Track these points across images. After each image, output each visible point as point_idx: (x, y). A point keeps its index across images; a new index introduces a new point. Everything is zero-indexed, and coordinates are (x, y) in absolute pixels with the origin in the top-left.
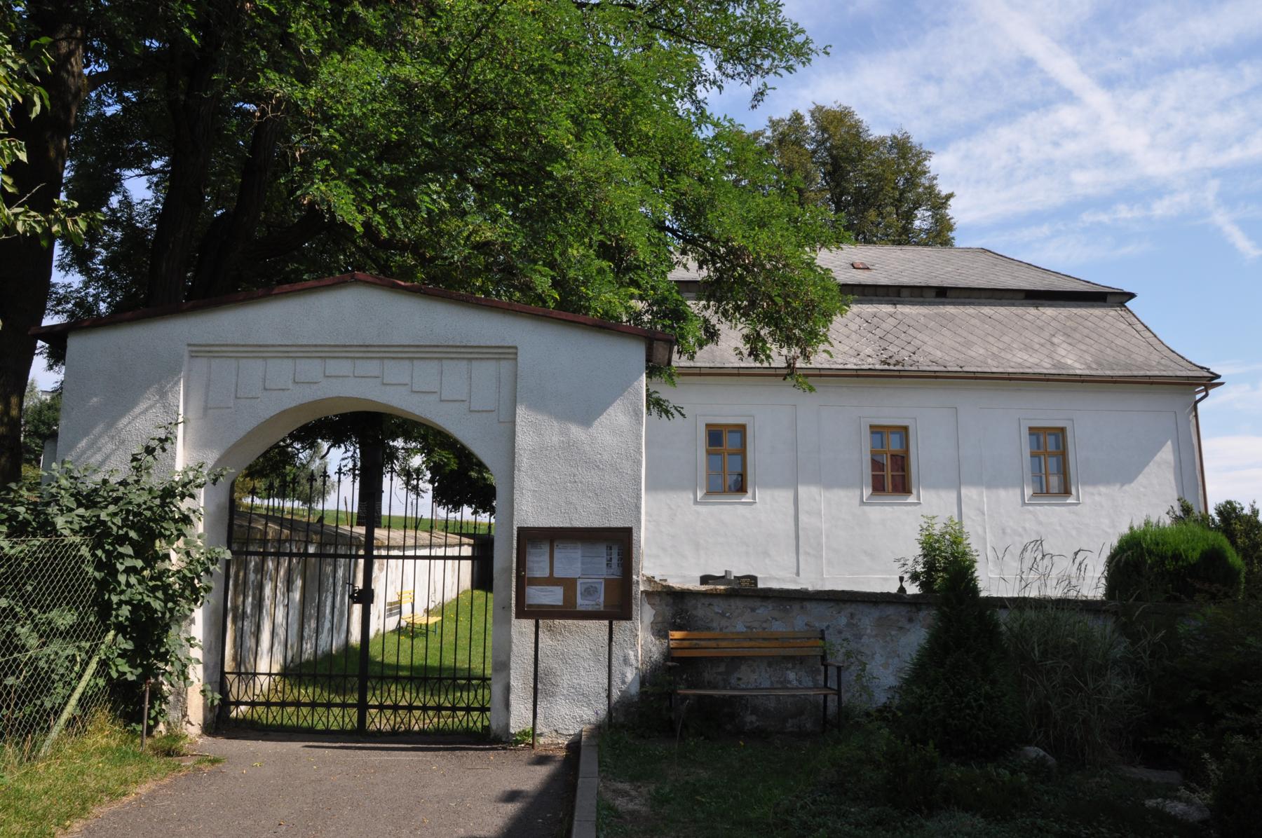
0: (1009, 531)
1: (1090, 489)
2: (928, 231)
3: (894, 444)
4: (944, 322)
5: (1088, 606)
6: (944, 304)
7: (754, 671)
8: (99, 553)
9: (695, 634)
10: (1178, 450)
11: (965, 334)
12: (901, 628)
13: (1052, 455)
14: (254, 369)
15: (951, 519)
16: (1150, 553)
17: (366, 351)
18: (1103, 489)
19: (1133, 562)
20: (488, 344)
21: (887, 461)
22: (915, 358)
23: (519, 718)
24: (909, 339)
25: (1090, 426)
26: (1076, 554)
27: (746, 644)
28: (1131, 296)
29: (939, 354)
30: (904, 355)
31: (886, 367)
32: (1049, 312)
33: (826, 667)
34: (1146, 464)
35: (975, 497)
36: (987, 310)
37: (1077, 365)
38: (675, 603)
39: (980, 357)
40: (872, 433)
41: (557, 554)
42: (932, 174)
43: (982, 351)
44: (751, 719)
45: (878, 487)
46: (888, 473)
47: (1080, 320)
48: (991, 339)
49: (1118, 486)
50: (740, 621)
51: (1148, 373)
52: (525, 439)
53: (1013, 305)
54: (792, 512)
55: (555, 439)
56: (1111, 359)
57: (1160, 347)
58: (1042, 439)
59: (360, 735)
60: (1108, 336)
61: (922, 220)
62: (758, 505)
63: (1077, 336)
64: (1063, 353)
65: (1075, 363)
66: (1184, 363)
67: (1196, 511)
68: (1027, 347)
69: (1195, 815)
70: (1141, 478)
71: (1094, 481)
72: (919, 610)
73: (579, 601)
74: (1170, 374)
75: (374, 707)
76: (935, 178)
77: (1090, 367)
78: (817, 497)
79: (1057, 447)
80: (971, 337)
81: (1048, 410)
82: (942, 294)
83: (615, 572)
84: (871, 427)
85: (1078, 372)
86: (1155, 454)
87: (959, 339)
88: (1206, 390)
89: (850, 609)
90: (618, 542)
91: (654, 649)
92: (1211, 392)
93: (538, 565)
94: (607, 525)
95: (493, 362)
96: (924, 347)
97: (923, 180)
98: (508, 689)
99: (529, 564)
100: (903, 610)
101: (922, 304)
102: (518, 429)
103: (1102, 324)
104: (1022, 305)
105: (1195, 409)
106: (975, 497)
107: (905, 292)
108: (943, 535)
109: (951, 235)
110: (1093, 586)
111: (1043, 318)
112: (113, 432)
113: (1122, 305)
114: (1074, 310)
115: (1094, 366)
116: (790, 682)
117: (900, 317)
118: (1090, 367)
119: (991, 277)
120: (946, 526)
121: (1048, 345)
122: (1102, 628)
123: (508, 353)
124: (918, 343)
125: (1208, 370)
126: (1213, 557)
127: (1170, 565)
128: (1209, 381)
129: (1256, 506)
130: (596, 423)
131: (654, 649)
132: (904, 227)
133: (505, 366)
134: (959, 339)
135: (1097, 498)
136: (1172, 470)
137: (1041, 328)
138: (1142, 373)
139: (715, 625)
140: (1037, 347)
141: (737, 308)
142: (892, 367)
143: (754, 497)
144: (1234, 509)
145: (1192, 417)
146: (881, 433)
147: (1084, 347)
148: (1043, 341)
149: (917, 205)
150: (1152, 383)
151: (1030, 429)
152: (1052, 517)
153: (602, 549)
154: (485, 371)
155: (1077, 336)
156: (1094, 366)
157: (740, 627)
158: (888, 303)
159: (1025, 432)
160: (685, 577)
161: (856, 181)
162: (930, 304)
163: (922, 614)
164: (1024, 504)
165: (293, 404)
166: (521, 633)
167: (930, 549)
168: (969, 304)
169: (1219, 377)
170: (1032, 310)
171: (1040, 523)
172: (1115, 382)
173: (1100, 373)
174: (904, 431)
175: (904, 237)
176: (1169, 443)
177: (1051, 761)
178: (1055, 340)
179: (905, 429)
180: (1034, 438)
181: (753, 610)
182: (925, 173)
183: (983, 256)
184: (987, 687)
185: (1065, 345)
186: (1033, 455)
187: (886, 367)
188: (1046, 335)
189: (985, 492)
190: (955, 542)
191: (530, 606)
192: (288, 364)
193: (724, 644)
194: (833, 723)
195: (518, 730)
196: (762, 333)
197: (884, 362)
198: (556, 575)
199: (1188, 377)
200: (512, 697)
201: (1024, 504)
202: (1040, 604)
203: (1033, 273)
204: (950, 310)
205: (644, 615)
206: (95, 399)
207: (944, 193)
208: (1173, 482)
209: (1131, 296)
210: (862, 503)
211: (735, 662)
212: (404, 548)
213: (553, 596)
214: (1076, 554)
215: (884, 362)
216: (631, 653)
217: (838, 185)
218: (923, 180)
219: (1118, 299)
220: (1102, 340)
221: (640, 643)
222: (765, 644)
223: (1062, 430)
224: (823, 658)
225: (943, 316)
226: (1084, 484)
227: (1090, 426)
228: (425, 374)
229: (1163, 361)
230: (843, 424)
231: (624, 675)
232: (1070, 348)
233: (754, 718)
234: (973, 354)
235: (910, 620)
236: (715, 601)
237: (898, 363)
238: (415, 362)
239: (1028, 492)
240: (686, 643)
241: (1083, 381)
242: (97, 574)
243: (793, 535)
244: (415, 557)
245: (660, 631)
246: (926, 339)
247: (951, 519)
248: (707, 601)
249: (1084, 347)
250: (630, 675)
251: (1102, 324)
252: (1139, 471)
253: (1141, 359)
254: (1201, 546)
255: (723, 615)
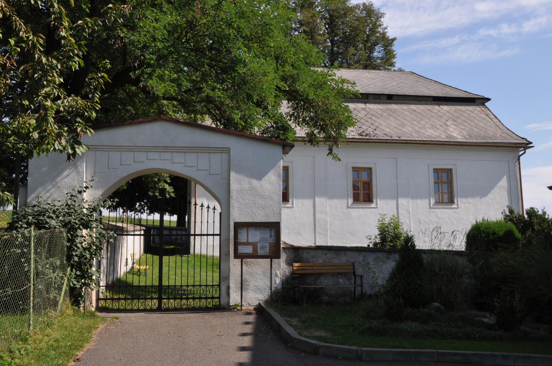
0: (422, 222)
1: (464, 200)
2: (382, 59)
3: (364, 177)
4: (391, 113)
5: (458, 253)
6: (391, 103)
7: (326, 279)
8: (69, 235)
9: (304, 264)
10: (509, 181)
11: (401, 120)
12: (384, 261)
13: (445, 183)
14: (116, 156)
15: (394, 216)
16: (484, 232)
17: (166, 149)
18: (470, 200)
19: (479, 236)
20: (218, 146)
21: (360, 185)
22: (376, 132)
23: (234, 298)
24: (373, 122)
25: (463, 167)
26: (453, 232)
27: (323, 268)
28: (488, 100)
29: (388, 130)
30: (370, 131)
31: (361, 137)
32: (445, 108)
33: (355, 276)
34: (493, 187)
35: (405, 204)
36: (413, 107)
37: (459, 137)
38: (296, 253)
39: (409, 132)
40: (353, 171)
41: (250, 233)
42: (384, 26)
43: (410, 129)
44: (325, 298)
45: (356, 199)
46: (361, 192)
47: (461, 112)
48: (415, 123)
49: (479, 198)
50: (321, 259)
51: (495, 141)
52: (234, 186)
53: (427, 104)
54: (312, 212)
55: (246, 186)
56: (476, 134)
57: (502, 127)
58: (440, 174)
59: (159, 309)
60: (476, 121)
61: (378, 53)
62: (295, 208)
63: (460, 121)
64: (452, 130)
65: (458, 135)
66: (514, 136)
67: (516, 212)
68: (433, 127)
69: (491, 322)
70: (490, 195)
71: (466, 196)
72: (391, 254)
73: (259, 251)
74: (507, 141)
75: (155, 298)
76: (386, 28)
77: (465, 138)
78: (325, 204)
79: (448, 179)
80: (404, 121)
81: (443, 160)
82: (390, 98)
83: (272, 240)
84: (353, 168)
85: (459, 140)
86: (497, 183)
87: (399, 123)
88: (525, 150)
89: (364, 254)
90: (275, 227)
91: (287, 271)
92: (527, 151)
93: (243, 237)
94: (268, 221)
95: (219, 154)
96: (381, 127)
97: (379, 29)
98: (228, 288)
99: (239, 237)
100: (385, 254)
101: (379, 103)
102: (231, 182)
103: (472, 115)
104: (432, 104)
105: (519, 159)
106: (405, 204)
107: (371, 97)
108: (389, 224)
109: (394, 60)
110: (460, 244)
111: (442, 111)
112: (54, 183)
113: (483, 104)
114: (458, 107)
115: (468, 137)
116: (340, 283)
117: (368, 110)
118: (465, 138)
119: (416, 88)
120: (392, 219)
121: (444, 126)
122: (462, 261)
123: (227, 150)
124: (377, 124)
125: (526, 139)
126: (509, 234)
127: (491, 237)
128: (526, 145)
129: (545, 210)
130: (263, 179)
131: (287, 271)
132: (368, 56)
133: (225, 156)
134: (399, 123)
135: (467, 205)
136: (506, 191)
137: (441, 117)
138: (492, 141)
139: (311, 261)
140: (438, 127)
141: (304, 120)
142: (364, 137)
143: (293, 204)
144: (534, 211)
145: (517, 164)
146: (358, 171)
147: (463, 127)
148: (442, 124)
149: (375, 44)
150: (497, 146)
151: (434, 169)
152: (445, 214)
153: (239, 231)
154: (216, 158)
155: (460, 121)
156: (468, 137)
157: (321, 261)
158: (362, 102)
159: (431, 171)
160: (304, 240)
161: (343, 29)
162: (384, 103)
163: (392, 256)
164: (430, 208)
165: (134, 171)
166: (234, 265)
167: (383, 231)
168: (404, 103)
169: (531, 143)
170: (437, 107)
171: (438, 218)
172: (478, 146)
173: (470, 141)
174: (369, 170)
175: (369, 64)
176: (505, 177)
177: (442, 308)
178: (448, 123)
179: (370, 169)
180: (436, 174)
181: (326, 255)
182: (380, 25)
183: (412, 77)
184: (419, 281)
185: (453, 126)
186: (435, 183)
187: (361, 137)
188: (443, 120)
189: (410, 201)
190: (396, 227)
191: (240, 253)
192: (131, 154)
193: (315, 268)
194: (359, 298)
195: (233, 304)
196: (315, 132)
197: (360, 135)
198: (249, 241)
199: (516, 143)
200: (231, 291)
201: (430, 208)
202: (439, 252)
203: (438, 86)
204: (394, 106)
205: (284, 256)
206: (44, 169)
207: (390, 38)
208: (507, 197)
209: (488, 100)
210: (348, 207)
211: (319, 275)
212: (134, 231)
213: (248, 250)
214: (453, 232)
215: (360, 135)
216: (278, 272)
217: (332, 31)
218: (379, 29)
219: (481, 101)
220: (472, 123)
221: (282, 268)
222: (331, 268)
223: (450, 170)
224: (354, 273)
225: (390, 110)
226: (461, 197)
227: (463, 167)
228: (191, 159)
229: (503, 135)
230: (338, 168)
231: (275, 281)
232: (455, 127)
233: (326, 298)
234: (405, 130)
235: (388, 258)
236: (311, 251)
237: (367, 135)
238: (186, 154)
239: (433, 201)
240: (300, 268)
241: (462, 145)
242: (67, 244)
243: (312, 223)
244: (134, 235)
245: (289, 263)
246: (382, 122)
247: (394, 216)
248: (307, 251)
249: (463, 127)
250: (278, 281)
251: (472, 115)
252: (489, 192)
253: (491, 134)
254: (504, 229)
255: (314, 256)
